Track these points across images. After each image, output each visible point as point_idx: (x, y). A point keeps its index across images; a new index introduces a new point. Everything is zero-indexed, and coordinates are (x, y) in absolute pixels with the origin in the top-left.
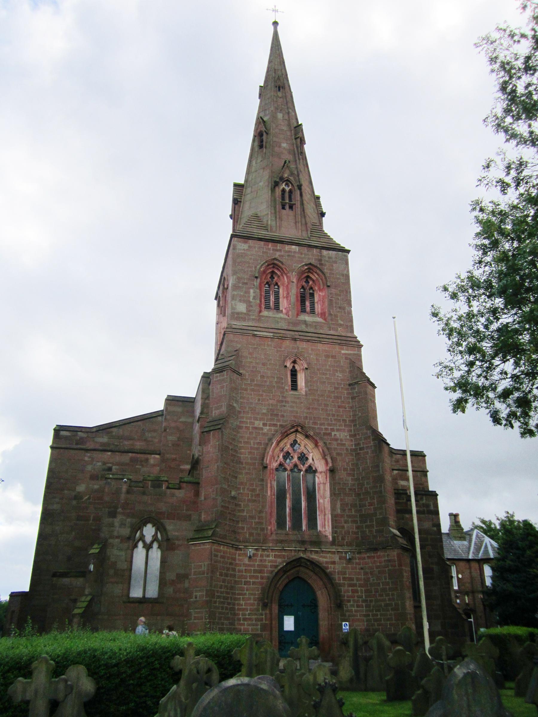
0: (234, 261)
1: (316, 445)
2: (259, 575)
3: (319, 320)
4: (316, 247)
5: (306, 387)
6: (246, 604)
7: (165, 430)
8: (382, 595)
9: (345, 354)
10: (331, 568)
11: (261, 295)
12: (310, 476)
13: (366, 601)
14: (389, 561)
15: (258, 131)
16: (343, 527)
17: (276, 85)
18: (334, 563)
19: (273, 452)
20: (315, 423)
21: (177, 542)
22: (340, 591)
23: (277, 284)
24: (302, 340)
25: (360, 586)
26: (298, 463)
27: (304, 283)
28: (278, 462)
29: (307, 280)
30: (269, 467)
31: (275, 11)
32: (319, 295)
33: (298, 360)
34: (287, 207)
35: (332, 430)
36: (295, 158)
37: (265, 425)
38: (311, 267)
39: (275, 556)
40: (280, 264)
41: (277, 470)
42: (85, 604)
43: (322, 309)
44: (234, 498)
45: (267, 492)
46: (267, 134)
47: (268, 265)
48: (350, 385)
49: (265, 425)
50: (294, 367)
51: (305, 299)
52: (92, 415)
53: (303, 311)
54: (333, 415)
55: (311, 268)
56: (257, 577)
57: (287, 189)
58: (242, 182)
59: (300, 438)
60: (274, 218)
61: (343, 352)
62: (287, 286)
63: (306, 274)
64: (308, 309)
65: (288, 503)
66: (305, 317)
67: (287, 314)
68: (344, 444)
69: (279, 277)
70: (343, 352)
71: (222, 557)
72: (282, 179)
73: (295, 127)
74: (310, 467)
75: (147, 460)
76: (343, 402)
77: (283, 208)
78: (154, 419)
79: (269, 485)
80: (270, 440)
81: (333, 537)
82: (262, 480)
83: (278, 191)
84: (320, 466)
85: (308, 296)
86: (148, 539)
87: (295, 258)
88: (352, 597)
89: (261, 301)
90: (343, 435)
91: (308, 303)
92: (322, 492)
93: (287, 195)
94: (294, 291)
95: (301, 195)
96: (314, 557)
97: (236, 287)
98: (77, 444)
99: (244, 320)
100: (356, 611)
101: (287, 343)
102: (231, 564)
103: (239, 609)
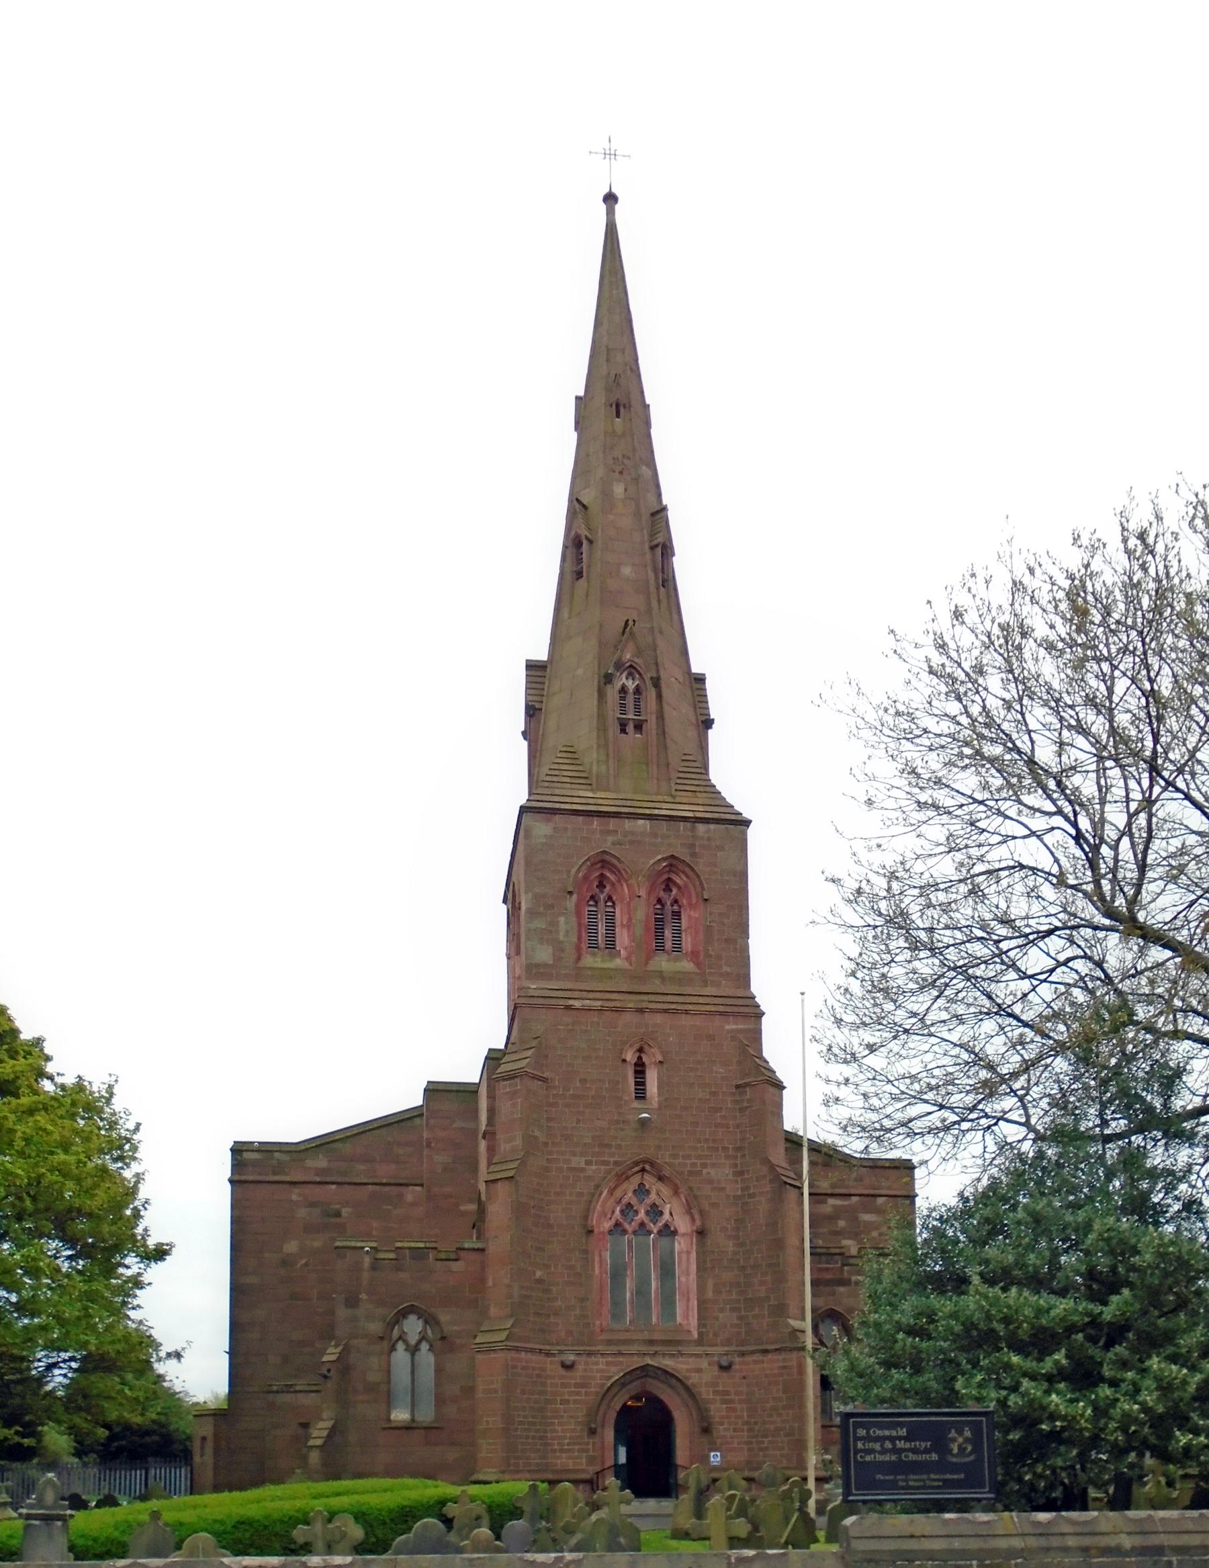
0: (528, 863)
1: (676, 1192)
2: (583, 1390)
3: (687, 966)
4: (685, 819)
5: (659, 1095)
6: (563, 1431)
7: (429, 1146)
8: (771, 1416)
9: (732, 1031)
10: (693, 1379)
11: (580, 925)
12: (665, 1241)
13: (747, 1423)
14: (784, 1367)
15: (573, 533)
16: (717, 1318)
17: (613, 408)
18: (699, 1370)
19: (603, 1206)
20: (674, 1156)
21: (458, 1341)
22: (707, 1410)
23: (610, 898)
24: (653, 1011)
25: (741, 1402)
26: (646, 1220)
27: (662, 894)
28: (613, 1221)
29: (667, 886)
30: (596, 1230)
31: (610, 155)
32: (690, 916)
33: (646, 1047)
34: (630, 728)
35: (704, 1165)
36: (649, 603)
37: (588, 1163)
38: (674, 862)
39: (608, 1363)
40: (615, 862)
41: (610, 1232)
42: (325, 1433)
43: (693, 945)
44: (539, 1281)
45: (593, 1270)
46: (590, 542)
47: (592, 865)
48: (737, 1087)
49: (588, 1163)
50: (640, 1058)
51: (663, 920)
52: (294, 1121)
53: (661, 948)
54: (706, 1140)
55: (673, 863)
56: (578, 1394)
57: (631, 685)
58: (542, 655)
59: (649, 1181)
60: (603, 758)
61: (727, 1027)
62: (629, 904)
63: (666, 876)
64: (669, 945)
65: (629, 1284)
66: (662, 963)
67: (628, 959)
68: (724, 1189)
69: (613, 885)
70: (727, 1027)
71: (524, 1368)
72: (619, 666)
73: (653, 515)
74: (666, 1226)
75: (400, 1196)
76: (724, 1117)
77: (623, 731)
78: (409, 1123)
79: (597, 1259)
80: (597, 1186)
81: (700, 1334)
82: (586, 1252)
83: (612, 693)
84: (682, 1224)
85: (669, 916)
86: (413, 1339)
87: (641, 850)
88: (728, 1417)
89: (579, 938)
90: (722, 1172)
91: (668, 933)
92: (684, 1265)
93: (630, 698)
94: (642, 912)
95: (659, 696)
96: (668, 1363)
97: (532, 913)
98: (275, 1173)
99: (549, 977)
100: (732, 1437)
101: (627, 1017)
102: (538, 1376)
103: (553, 1439)
